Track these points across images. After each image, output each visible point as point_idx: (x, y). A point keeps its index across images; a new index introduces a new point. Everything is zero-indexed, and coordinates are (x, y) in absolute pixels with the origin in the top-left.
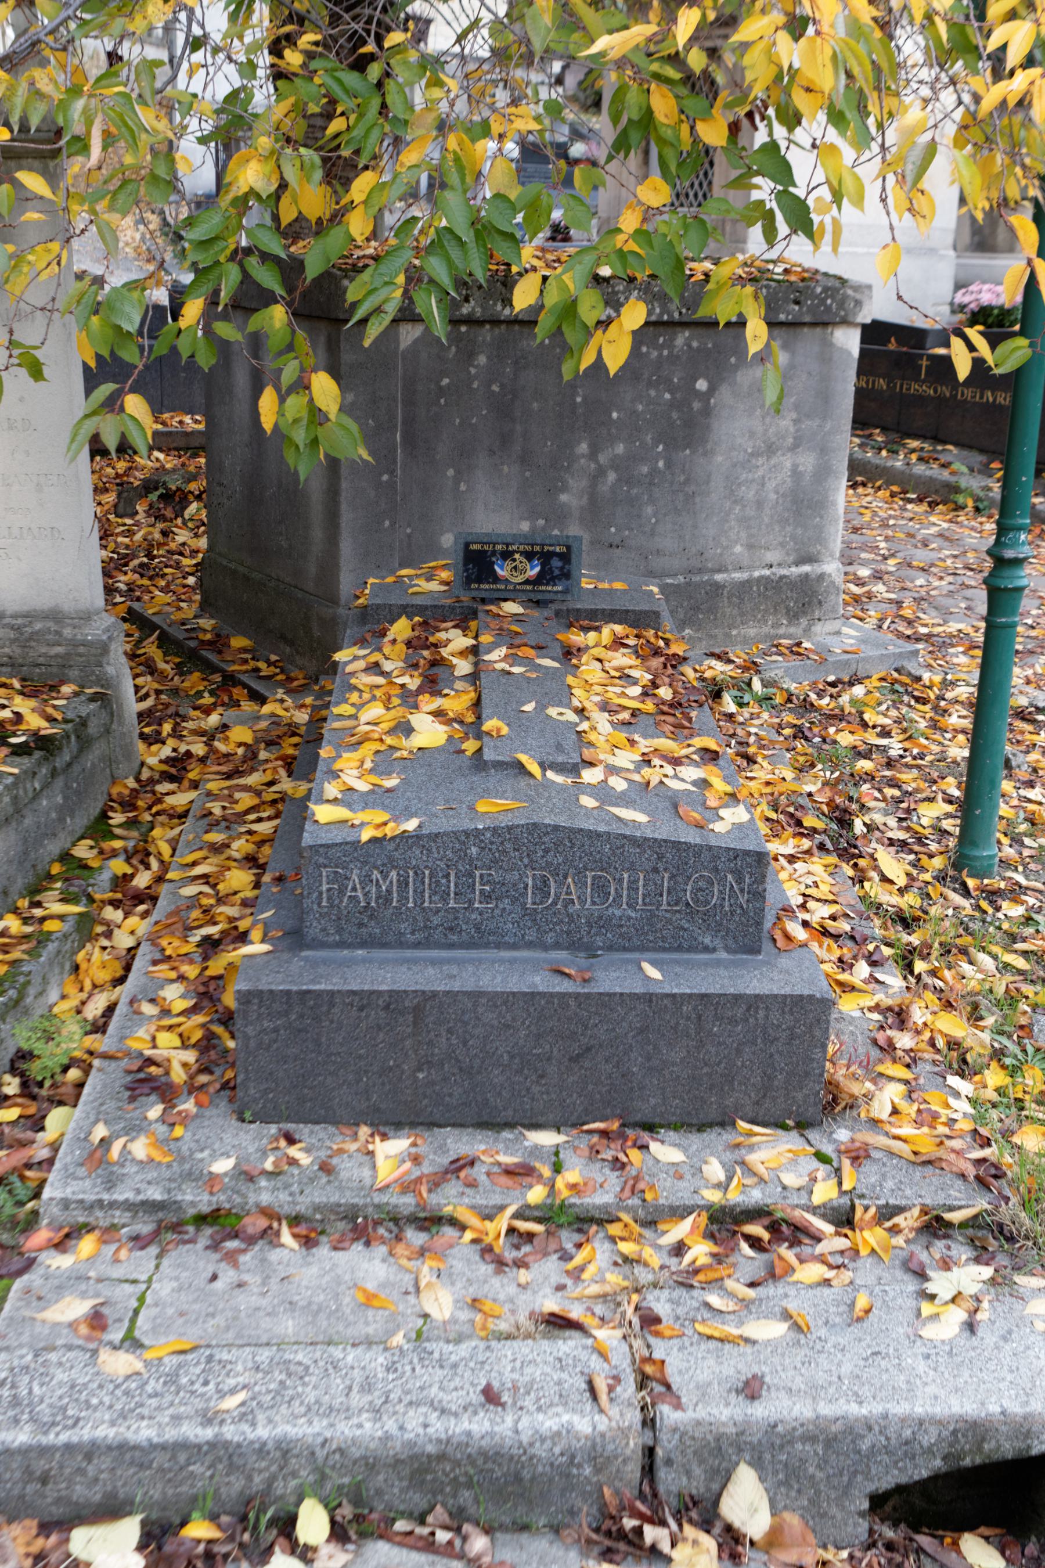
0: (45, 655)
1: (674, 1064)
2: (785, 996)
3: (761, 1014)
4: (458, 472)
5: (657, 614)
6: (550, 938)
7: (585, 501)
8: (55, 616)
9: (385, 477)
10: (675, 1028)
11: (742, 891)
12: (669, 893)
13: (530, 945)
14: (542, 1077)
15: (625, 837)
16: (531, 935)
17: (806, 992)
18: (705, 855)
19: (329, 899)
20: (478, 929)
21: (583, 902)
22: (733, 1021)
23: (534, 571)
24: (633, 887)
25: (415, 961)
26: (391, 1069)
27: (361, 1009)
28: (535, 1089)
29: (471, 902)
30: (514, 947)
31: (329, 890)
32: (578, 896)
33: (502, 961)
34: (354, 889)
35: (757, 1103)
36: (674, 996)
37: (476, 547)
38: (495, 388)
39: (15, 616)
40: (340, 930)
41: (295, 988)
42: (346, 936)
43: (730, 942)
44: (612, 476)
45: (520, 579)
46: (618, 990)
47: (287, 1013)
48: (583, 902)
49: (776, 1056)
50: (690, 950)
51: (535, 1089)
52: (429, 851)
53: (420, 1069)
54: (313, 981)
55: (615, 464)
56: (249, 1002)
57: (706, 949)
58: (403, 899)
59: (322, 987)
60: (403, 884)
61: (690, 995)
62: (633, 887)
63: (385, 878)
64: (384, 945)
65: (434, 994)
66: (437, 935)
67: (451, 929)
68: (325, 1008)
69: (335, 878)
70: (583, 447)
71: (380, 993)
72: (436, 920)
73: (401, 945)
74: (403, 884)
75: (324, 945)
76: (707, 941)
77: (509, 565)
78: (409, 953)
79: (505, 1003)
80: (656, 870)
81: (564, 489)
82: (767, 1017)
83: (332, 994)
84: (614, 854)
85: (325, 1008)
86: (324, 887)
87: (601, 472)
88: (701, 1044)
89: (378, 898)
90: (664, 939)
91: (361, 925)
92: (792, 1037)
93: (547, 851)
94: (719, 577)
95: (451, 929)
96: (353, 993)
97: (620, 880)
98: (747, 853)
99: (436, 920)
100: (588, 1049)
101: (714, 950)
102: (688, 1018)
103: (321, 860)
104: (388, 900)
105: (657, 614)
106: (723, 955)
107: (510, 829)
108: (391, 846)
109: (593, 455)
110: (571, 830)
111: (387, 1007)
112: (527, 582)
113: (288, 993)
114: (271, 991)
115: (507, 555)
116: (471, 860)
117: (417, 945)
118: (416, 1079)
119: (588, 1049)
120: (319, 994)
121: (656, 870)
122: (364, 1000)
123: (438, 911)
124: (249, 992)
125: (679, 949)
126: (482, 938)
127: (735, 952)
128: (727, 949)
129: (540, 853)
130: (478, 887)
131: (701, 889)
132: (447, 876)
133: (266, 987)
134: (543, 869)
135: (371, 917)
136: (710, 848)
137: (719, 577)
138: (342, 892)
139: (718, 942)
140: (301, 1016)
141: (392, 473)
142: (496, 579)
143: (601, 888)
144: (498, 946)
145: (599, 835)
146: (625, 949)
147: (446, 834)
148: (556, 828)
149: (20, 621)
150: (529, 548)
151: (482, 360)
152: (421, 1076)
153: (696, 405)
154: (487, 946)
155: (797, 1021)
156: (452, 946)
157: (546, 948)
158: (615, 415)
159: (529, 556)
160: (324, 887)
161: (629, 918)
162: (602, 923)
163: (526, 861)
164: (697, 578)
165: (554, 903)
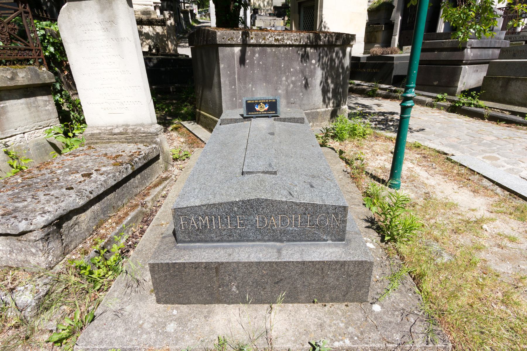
0: (140, 136)
1: (313, 284)
2: (356, 261)
3: (346, 267)
4: (252, 85)
5: (303, 119)
6: (266, 238)
7: (285, 92)
8: (142, 125)
9: (233, 87)
10: (313, 273)
11: (338, 220)
12: (310, 221)
13: (259, 240)
14: (264, 289)
15: (293, 202)
16: (260, 237)
17: (364, 259)
18: (324, 208)
19: (184, 227)
20: (240, 236)
21: (278, 226)
22: (335, 270)
23: (266, 108)
24: (296, 219)
25: (216, 247)
26: (209, 287)
27: (196, 268)
28: (262, 293)
29: (236, 226)
30: (253, 241)
31: (184, 224)
32: (276, 222)
33: (249, 246)
34: (193, 223)
35: (344, 296)
36: (313, 262)
37: (250, 102)
38: (261, 63)
39: (132, 126)
40: (190, 237)
41: (170, 262)
42: (192, 239)
43: (333, 238)
44: (291, 86)
45: (263, 110)
46: (292, 260)
47: (169, 270)
48: (278, 226)
49: (352, 281)
50: (318, 241)
51: (262, 293)
52: (219, 209)
53: (220, 287)
54: (178, 259)
55: (293, 82)
56: (154, 267)
57: (324, 240)
58: (211, 225)
59: (181, 261)
60: (211, 221)
61: (319, 262)
62: (296, 219)
63: (204, 219)
64: (206, 242)
65: (222, 263)
66: (225, 238)
67: (230, 235)
68: (182, 269)
69: (185, 220)
70: (284, 78)
71: (202, 263)
72: (224, 233)
73: (213, 241)
74: (211, 221)
75: (184, 242)
76: (325, 237)
77: (259, 107)
78: (215, 244)
79: (249, 265)
80: (305, 214)
81: (280, 89)
82: (348, 268)
83: (184, 264)
84: (289, 208)
85: (182, 269)
86: (182, 223)
87: (289, 85)
88: (324, 277)
89: (202, 226)
90: (308, 237)
91: (197, 235)
92: (358, 275)
93: (263, 208)
94: (318, 110)
95: (230, 235)
96: (193, 263)
97: (292, 218)
98: (340, 207)
99: (224, 233)
100: (282, 280)
101: (327, 240)
102: (318, 269)
103: (179, 214)
104: (206, 227)
105: (303, 119)
106: (330, 242)
107: (248, 201)
108: (205, 208)
109: (286, 81)
110: (272, 200)
111: (205, 268)
112: (265, 111)
113: (168, 264)
114: (162, 263)
115: (258, 104)
116: (235, 212)
117: (218, 241)
118: (219, 290)
119: (282, 280)
120: (179, 264)
121: (305, 214)
122: (196, 266)
123: (225, 230)
124: (154, 264)
125: (314, 240)
126: (242, 238)
127: (335, 241)
128: (332, 240)
129: (261, 209)
130: (238, 221)
131: (322, 220)
132: (227, 218)
133: (159, 262)
134: (262, 214)
135: (200, 232)
136: (326, 205)
137: (318, 110)
138: (189, 224)
139: (328, 238)
140: (174, 271)
141: (235, 85)
142: (256, 111)
143: (283, 220)
144: (248, 241)
145: (283, 202)
146: (294, 241)
147: (225, 203)
148: (266, 200)
149: (134, 127)
150: (264, 101)
151: (257, 55)
152: (220, 289)
153: (312, 67)
154: (243, 241)
155: (360, 269)
156: (230, 241)
157: (265, 241)
158: (292, 70)
159: (265, 103)
160: (182, 223)
161: (295, 231)
162: (284, 232)
163: (256, 212)
164: (313, 111)
165: (267, 226)
